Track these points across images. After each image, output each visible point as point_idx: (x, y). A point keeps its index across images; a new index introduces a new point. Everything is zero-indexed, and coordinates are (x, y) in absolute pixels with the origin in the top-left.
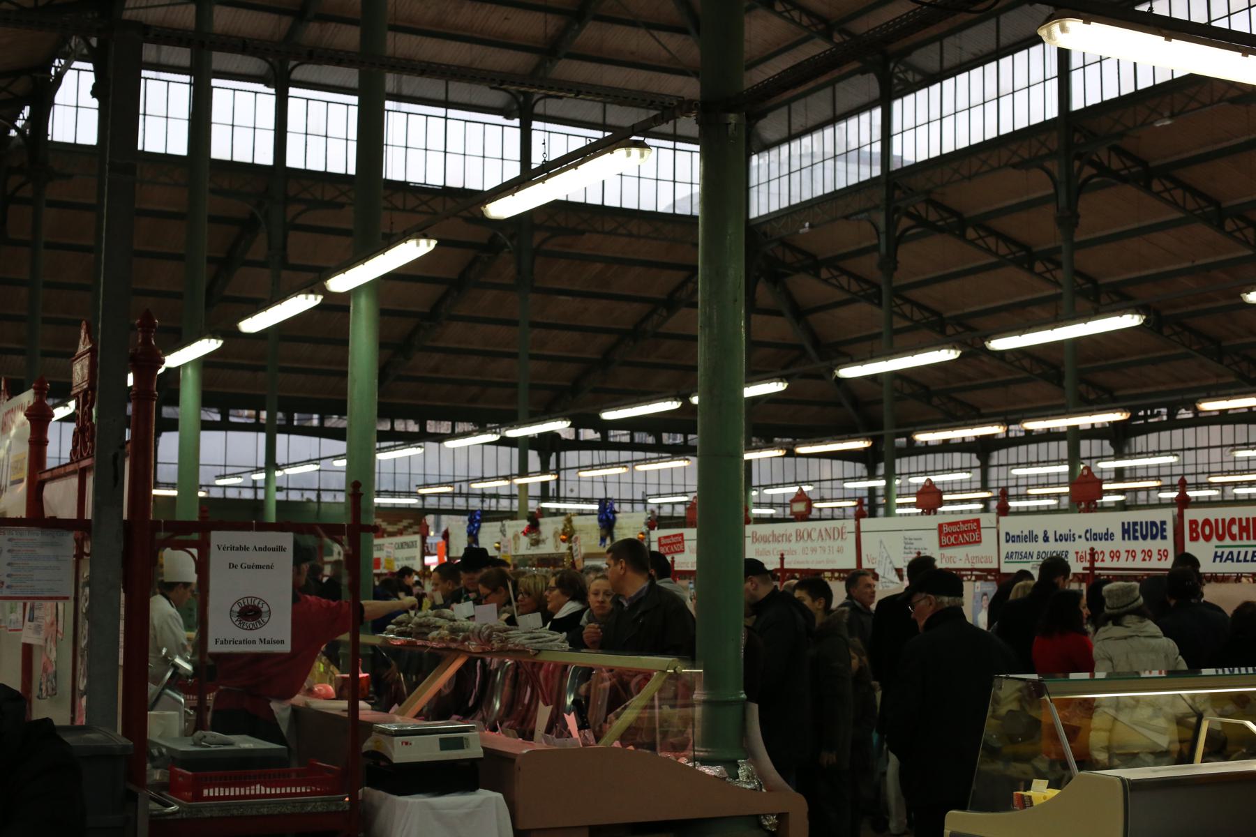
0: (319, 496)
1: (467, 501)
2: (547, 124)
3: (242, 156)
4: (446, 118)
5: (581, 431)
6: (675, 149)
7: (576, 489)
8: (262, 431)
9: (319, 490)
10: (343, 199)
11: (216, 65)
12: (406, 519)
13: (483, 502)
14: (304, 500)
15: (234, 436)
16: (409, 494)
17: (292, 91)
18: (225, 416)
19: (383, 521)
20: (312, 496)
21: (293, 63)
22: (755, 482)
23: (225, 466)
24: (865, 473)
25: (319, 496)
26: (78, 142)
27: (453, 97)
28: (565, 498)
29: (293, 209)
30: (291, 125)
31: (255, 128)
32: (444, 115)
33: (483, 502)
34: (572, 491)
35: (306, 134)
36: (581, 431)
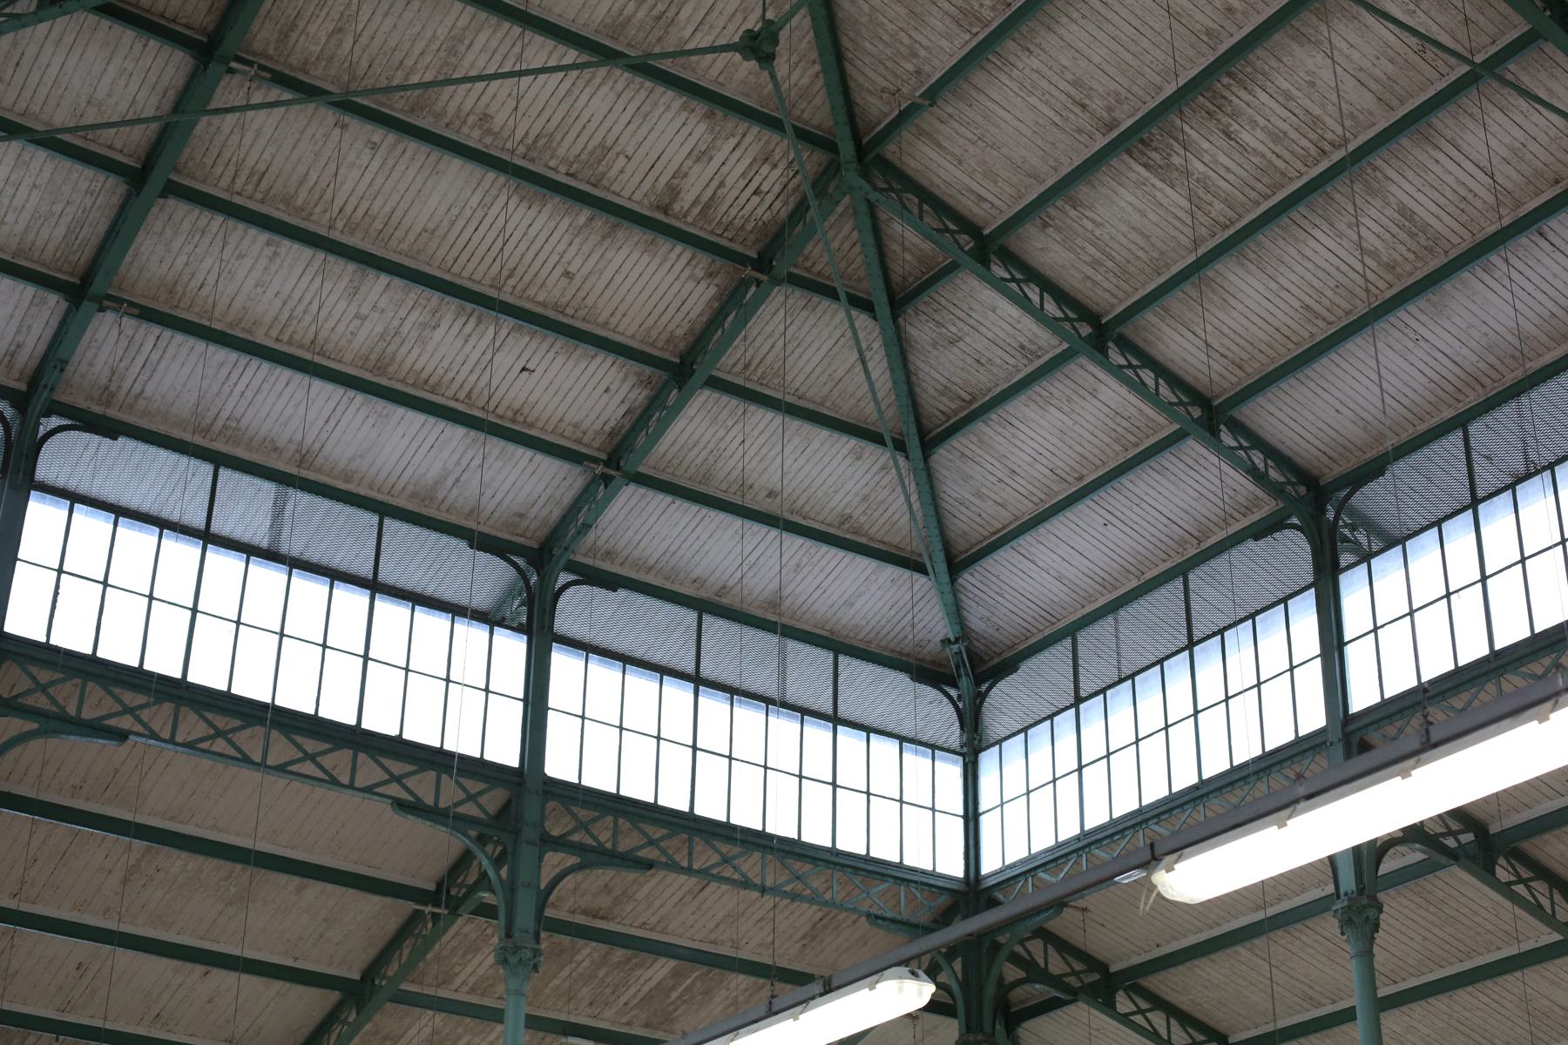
10: (126, 722)
21: (55, 421)
30: (555, 698)
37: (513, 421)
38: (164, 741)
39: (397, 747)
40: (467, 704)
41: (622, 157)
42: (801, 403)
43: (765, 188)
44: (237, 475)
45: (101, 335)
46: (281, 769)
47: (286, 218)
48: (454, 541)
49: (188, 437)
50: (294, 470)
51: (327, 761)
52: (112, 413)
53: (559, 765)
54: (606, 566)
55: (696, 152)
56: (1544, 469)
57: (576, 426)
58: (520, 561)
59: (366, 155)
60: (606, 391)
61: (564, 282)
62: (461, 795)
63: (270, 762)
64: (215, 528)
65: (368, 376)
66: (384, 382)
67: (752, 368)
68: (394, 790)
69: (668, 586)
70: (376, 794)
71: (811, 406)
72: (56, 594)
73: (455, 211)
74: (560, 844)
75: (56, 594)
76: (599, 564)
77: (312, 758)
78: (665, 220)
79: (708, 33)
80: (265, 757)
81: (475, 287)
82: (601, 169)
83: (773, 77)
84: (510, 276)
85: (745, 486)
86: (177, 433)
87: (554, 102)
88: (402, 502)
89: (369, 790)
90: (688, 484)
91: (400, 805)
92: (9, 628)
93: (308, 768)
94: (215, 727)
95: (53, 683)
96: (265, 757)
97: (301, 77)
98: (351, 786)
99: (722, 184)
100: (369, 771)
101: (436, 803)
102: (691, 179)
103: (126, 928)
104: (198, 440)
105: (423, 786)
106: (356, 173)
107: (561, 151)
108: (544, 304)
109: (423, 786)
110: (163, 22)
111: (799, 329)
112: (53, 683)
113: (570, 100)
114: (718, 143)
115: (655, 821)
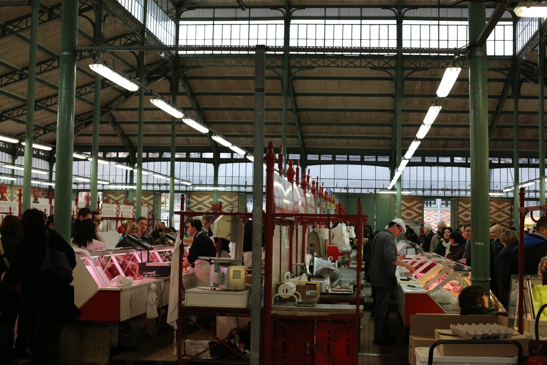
0: (375, 191)
1: (466, 193)
2: (448, 21)
3: (499, 53)
4: (361, 25)
5: (290, 155)
6: (213, 24)
7: (499, 186)
8: (469, 167)
9: (375, 189)
10: (314, 65)
11: (407, 14)
12: (415, 200)
13: (452, 192)
14: (369, 193)
15: (338, 166)
16: (501, 191)
17: (405, 22)
18: (188, 155)
19: (227, 197)
20: (373, 191)
21: (293, 9)
22: (520, 181)
23: (375, 180)
24: (10, 161)
25: (375, 191)
26: (505, 55)
27: (364, 15)
28: (493, 190)
29: (407, 72)
30: (404, 37)
31: (388, 39)
32: (212, 23)
33: (452, 192)
34: (497, 187)
35: (448, 40)
36: (290, 155)
38: (322, 67)
44: (330, 9)
49: (319, 4)
50: (341, 4)
51: (318, 62)
54: (415, 4)
56: (247, 7)
58: (394, 9)
62: (300, 62)
63: (343, 66)
64: (363, 15)
68: (369, 65)
74: (408, 68)
76: (412, 4)
77: (352, 63)
80: (360, 65)
86: (316, 4)
89: (364, 67)
91: (371, 68)
95: (300, 61)
96: (360, 65)
101: (420, 66)
103: (329, 108)
104: (321, 4)
105: (376, 63)
109: (376, 63)
112: (300, 61)
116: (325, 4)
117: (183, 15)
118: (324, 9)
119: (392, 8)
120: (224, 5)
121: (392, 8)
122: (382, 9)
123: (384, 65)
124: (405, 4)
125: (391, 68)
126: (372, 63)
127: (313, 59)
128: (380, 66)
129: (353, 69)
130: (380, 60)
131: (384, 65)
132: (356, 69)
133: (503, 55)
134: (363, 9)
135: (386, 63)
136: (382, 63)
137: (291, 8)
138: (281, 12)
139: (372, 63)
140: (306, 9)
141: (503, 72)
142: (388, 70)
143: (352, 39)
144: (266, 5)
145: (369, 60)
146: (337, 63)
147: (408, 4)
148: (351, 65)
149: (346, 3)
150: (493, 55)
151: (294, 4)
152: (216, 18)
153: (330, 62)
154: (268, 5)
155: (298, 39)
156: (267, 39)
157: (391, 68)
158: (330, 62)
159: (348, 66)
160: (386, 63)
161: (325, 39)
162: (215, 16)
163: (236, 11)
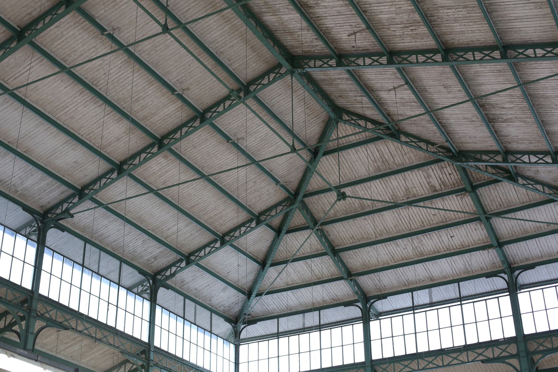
6: (461, 304)
21: (517, 272)
26: (395, 355)
37: (464, 247)
39: (479, 345)
40: (496, 324)
41: (413, 189)
42: (525, 204)
43: (450, 172)
45: (364, 280)
46: (448, 365)
47: (366, 242)
48: (481, 279)
49: (403, 288)
52: (384, 292)
53: (528, 329)
54: (529, 262)
55: (426, 177)
57: (479, 240)
59: (366, 221)
60: (476, 230)
61: (435, 217)
65: (421, 258)
66: (425, 257)
67: (502, 205)
68: (481, 358)
69: (551, 258)
70: (451, 365)
71: (528, 204)
72: (382, 345)
73: (396, 219)
75: (382, 345)
78: (438, 193)
79: (396, 157)
81: (418, 230)
82: (412, 193)
83: (349, 197)
84: (423, 223)
85: (526, 232)
86: (400, 289)
87: (386, 189)
88: (463, 276)
89: (423, 369)
90: (523, 236)
91: (483, 361)
92: (373, 358)
93: (431, 365)
94: (408, 367)
97: (336, 218)
98: (443, 366)
99: (440, 179)
100: (472, 355)
102: (433, 182)
105: (489, 353)
106: (368, 226)
107: (400, 196)
108: (437, 223)
109: (489, 353)
110: (303, 226)
111: (501, 191)
113: (388, 187)
114: (428, 172)
115: (540, 338)
116: (411, 287)
117: (243, 335)
118: (410, 293)
119: (356, 304)
120: (289, 312)
121: (356, 304)
122: (487, 278)
123: (501, 353)
124: (516, 265)
125: (512, 356)
126: (483, 354)
127: (477, 351)
128: (496, 356)
129: (458, 366)
130: (495, 348)
131: (501, 353)
132: (438, 370)
133: (535, 332)
134: (461, 283)
135: (504, 350)
136: (497, 352)
137: (369, 301)
138: (501, 279)
139: (483, 354)
140: (388, 298)
141: (507, 361)
142: (507, 361)
143: (451, 327)
144: (338, 302)
145: (480, 351)
146: (460, 358)
147: (520, 264)
148: (431, 365)
149: (437, 280)
150: (490, 340)
151: (372, 295)
152: (464, 297)
153: (451, 359)
154: (341, 302)
155: (533, 312)
156: (546, 310)
157: (512, 356)
158: (451, 359)
159: (452, 363)
160: (504, 350)
161: (464, 324)
162: (415, 304)
163: (304, 316)
